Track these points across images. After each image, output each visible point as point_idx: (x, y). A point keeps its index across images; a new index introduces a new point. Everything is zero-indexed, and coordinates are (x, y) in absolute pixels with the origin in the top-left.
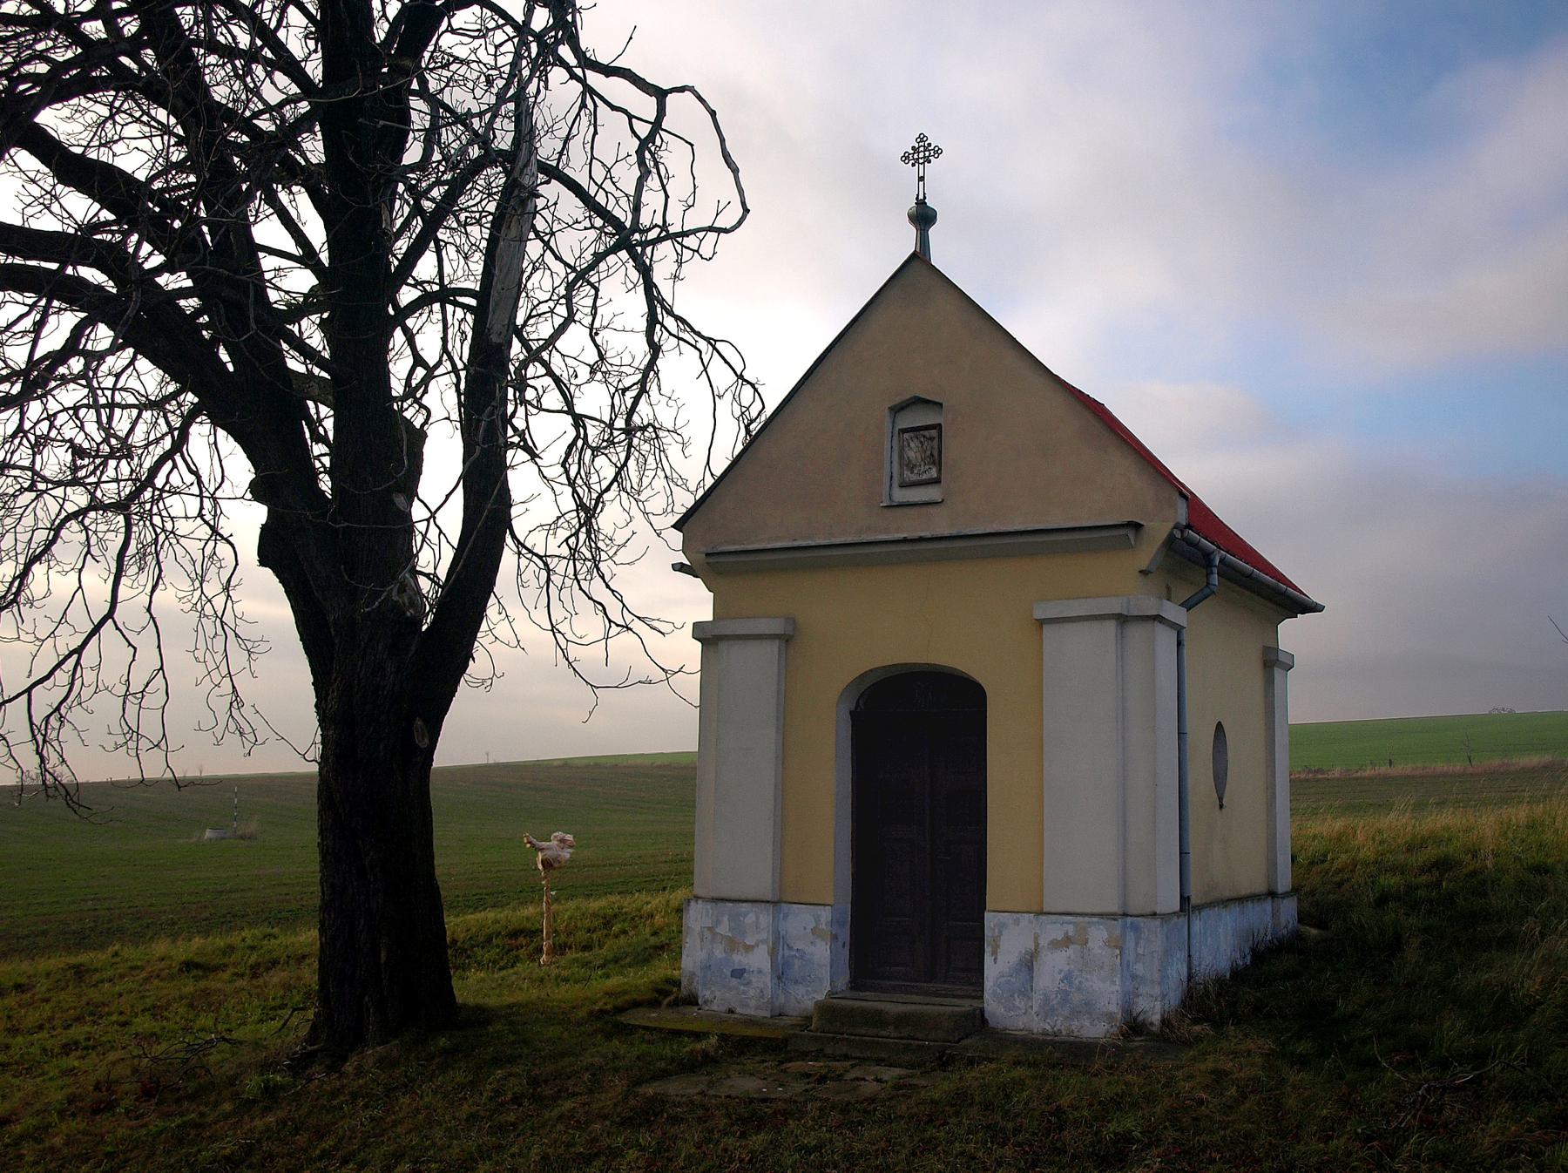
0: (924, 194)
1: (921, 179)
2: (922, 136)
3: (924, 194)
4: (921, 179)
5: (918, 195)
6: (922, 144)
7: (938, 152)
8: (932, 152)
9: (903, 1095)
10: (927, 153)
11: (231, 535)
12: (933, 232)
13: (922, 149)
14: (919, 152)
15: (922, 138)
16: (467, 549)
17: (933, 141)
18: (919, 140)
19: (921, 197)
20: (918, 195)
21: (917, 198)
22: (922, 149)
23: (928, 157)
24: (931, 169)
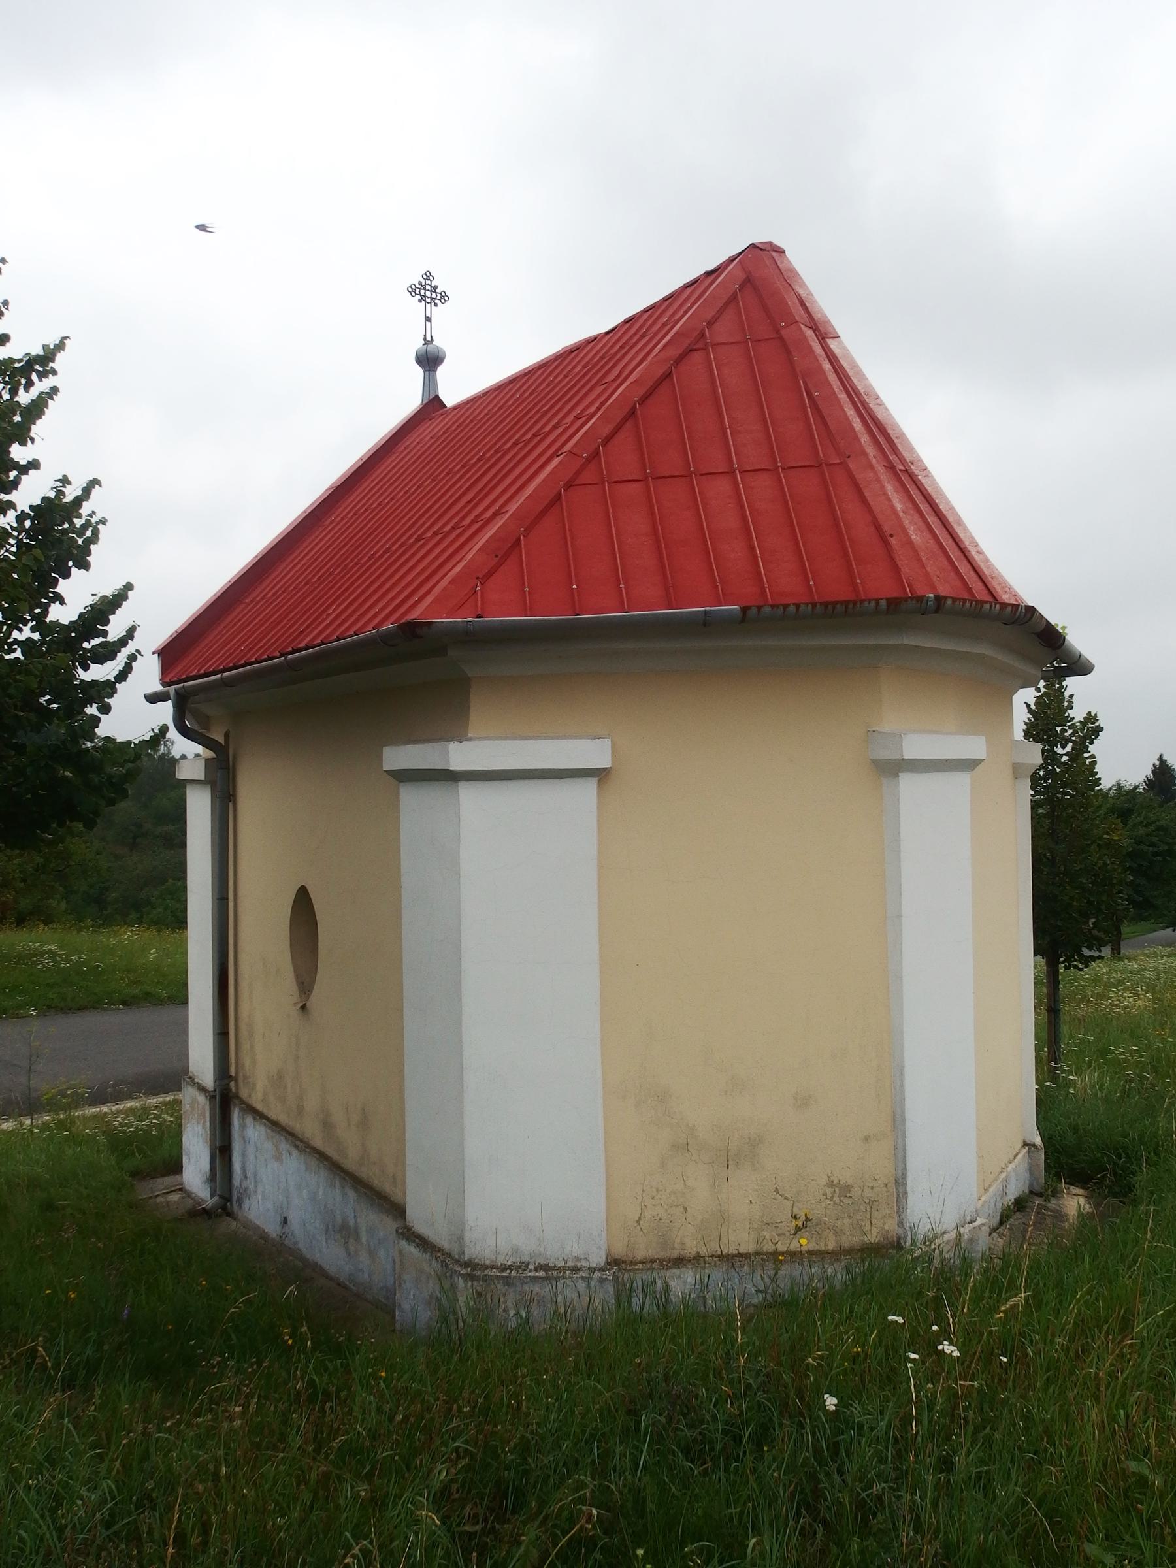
0: (431, 337)
1: (428, 319)
2: (410, 290)
3: (431, 337)
4: (428, 319)
5: (425, 335)
6: (418, 290)
7: (428, 276)
8: (428, 282)
9: (802, 1399)
10: (428, 287)
11: (429, 361)
12: (441, 371)
13: (422, 292)
14: (431, 291)
15: (412, 290)
16: (726, 417)
17: (416, 278)
18: (413, 294)
19: (428, 338)
20: (425, 335)
21: (425, 339)
22: (422, 292)
23: (431, 287)
24: (438, 312)
